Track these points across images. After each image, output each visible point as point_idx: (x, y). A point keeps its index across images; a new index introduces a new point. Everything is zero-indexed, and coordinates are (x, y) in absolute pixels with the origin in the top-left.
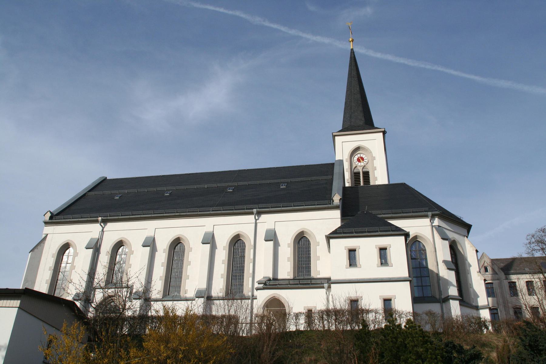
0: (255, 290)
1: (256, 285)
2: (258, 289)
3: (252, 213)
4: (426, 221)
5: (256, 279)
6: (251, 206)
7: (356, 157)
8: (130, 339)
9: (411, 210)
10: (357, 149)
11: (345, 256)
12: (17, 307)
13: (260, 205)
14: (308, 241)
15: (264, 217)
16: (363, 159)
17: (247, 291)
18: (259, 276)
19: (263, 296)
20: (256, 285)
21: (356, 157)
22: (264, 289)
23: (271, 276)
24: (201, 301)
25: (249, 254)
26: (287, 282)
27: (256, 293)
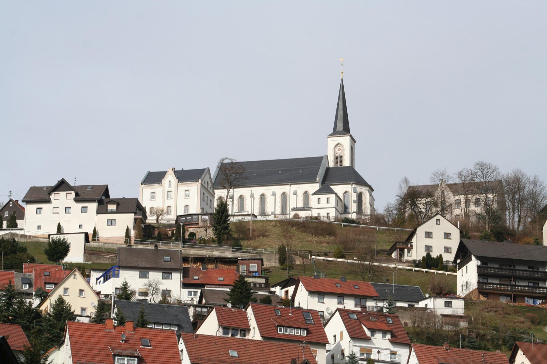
0: (378, 350)
1: (291, 210)
2: (291, 211)
3: (288, 185)
4: (350, 186)
5: (291, 208)
6: (289, 182)
7: (337, 149)
8: (50, 312)
9: (324, 192)
10: (338, 144)
11: (326, 199)
12: (275, 210)
13: (292, 182)
14: (308, 194)
15: (292, 186)
16: (340, 149)
17: (288, 212)
18: (292, 207)
19: (292, 213)
20: (291, 210)
21: (337, 149)
22: (293, 211)
23: (295, 207)
24: (273, 216)
25: (288, 199)
26: (300, 209)
27: (291, 212)
